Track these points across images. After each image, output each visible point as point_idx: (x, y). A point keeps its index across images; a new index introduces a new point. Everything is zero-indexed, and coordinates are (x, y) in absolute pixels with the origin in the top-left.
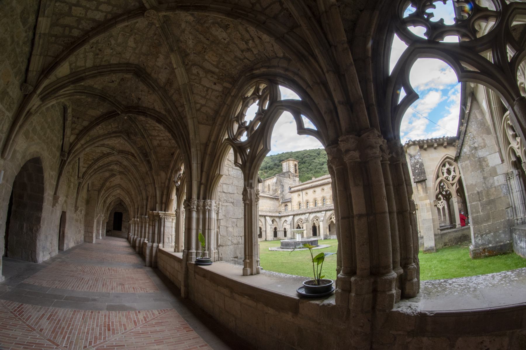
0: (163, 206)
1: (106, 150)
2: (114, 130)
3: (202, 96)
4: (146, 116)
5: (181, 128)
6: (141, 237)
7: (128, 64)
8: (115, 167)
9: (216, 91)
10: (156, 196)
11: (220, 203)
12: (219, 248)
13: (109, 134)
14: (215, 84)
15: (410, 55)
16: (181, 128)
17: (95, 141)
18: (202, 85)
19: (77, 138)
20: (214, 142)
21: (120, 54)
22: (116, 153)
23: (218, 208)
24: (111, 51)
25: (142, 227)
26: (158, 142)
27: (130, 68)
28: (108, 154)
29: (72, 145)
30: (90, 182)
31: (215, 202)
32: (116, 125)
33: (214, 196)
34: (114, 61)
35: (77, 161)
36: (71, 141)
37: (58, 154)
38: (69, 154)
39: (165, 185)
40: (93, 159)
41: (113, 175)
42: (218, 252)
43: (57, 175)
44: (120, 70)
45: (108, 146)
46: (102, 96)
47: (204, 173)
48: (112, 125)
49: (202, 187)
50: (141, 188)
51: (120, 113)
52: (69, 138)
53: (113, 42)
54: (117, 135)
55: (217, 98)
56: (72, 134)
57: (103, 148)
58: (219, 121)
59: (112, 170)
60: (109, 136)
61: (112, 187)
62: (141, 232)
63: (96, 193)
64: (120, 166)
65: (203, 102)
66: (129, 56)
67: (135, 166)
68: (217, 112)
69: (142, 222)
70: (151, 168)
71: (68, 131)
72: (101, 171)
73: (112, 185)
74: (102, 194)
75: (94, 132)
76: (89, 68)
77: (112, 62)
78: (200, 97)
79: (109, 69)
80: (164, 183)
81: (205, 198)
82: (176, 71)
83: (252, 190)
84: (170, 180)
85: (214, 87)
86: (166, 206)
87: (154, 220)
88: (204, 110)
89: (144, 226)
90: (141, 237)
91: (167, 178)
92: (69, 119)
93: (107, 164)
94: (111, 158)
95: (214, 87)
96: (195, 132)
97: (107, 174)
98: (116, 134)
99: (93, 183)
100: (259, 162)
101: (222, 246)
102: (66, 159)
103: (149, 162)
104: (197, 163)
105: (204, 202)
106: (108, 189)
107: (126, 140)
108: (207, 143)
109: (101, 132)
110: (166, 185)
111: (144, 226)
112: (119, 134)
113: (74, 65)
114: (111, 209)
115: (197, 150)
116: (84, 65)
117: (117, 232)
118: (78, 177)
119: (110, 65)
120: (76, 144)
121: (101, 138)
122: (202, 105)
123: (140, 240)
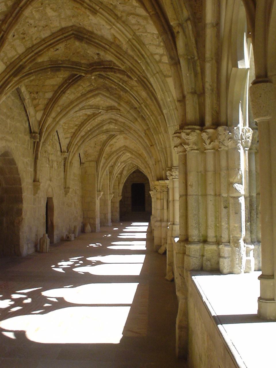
1: (89, 112)
2: (88, 89)
3: (156, 45)
7: (63, 30)
8: (112, 126)
13: (83, 95)
17: (67, 110)
18: (148, 33)
19: (44, 114)
21: (46, 26)
22: (103, 112)
24: (36, 29)
27: (67, 34)
28: (94, 115)
29: (41, 124)
30: (81, 152)
32: (88, 84)
34: (45, 34)
35: (56, 134)
36: (39, 118)
37: (27, 138)
38: (40, 133)
40: (76, 126)
41: (112, 137)
43: (33, 160)
44: (57, 41)
45: (91, 107)
46: (55, 67)
48: (83, 87)
51: (83, 74)
52: (35, 116)
53: (32, 21)
54: (94, 93)
56: (36, 111)
57: (84, 112)
59: (107, 131)
60: (85, 98)
61: (115, 151)
63: (93, 164)
64: (115, 123)
66: (57, 25)
71: (31, 111)
72: (90, 137)
73: (114, 149)
74: (101, 165)
75: (65, 99)
76: (22, 54)
77: (43, 37)
78: (154, 47)
79: (45, 45)
92: (27, 101)
93: (97, 125)
94: (99, 119)
97: (104, 137)
98: (93, 92)
99: (85, 153)
102: (38, 140)
106: (110, 155)
109: (72, 97)
112: (96, 92)
113: (6, 58)
114: (124, 180)
116: (16, 53)
118: (61, 152)
119: (44, 40)
120: (45, 121)
121: (75, 104)
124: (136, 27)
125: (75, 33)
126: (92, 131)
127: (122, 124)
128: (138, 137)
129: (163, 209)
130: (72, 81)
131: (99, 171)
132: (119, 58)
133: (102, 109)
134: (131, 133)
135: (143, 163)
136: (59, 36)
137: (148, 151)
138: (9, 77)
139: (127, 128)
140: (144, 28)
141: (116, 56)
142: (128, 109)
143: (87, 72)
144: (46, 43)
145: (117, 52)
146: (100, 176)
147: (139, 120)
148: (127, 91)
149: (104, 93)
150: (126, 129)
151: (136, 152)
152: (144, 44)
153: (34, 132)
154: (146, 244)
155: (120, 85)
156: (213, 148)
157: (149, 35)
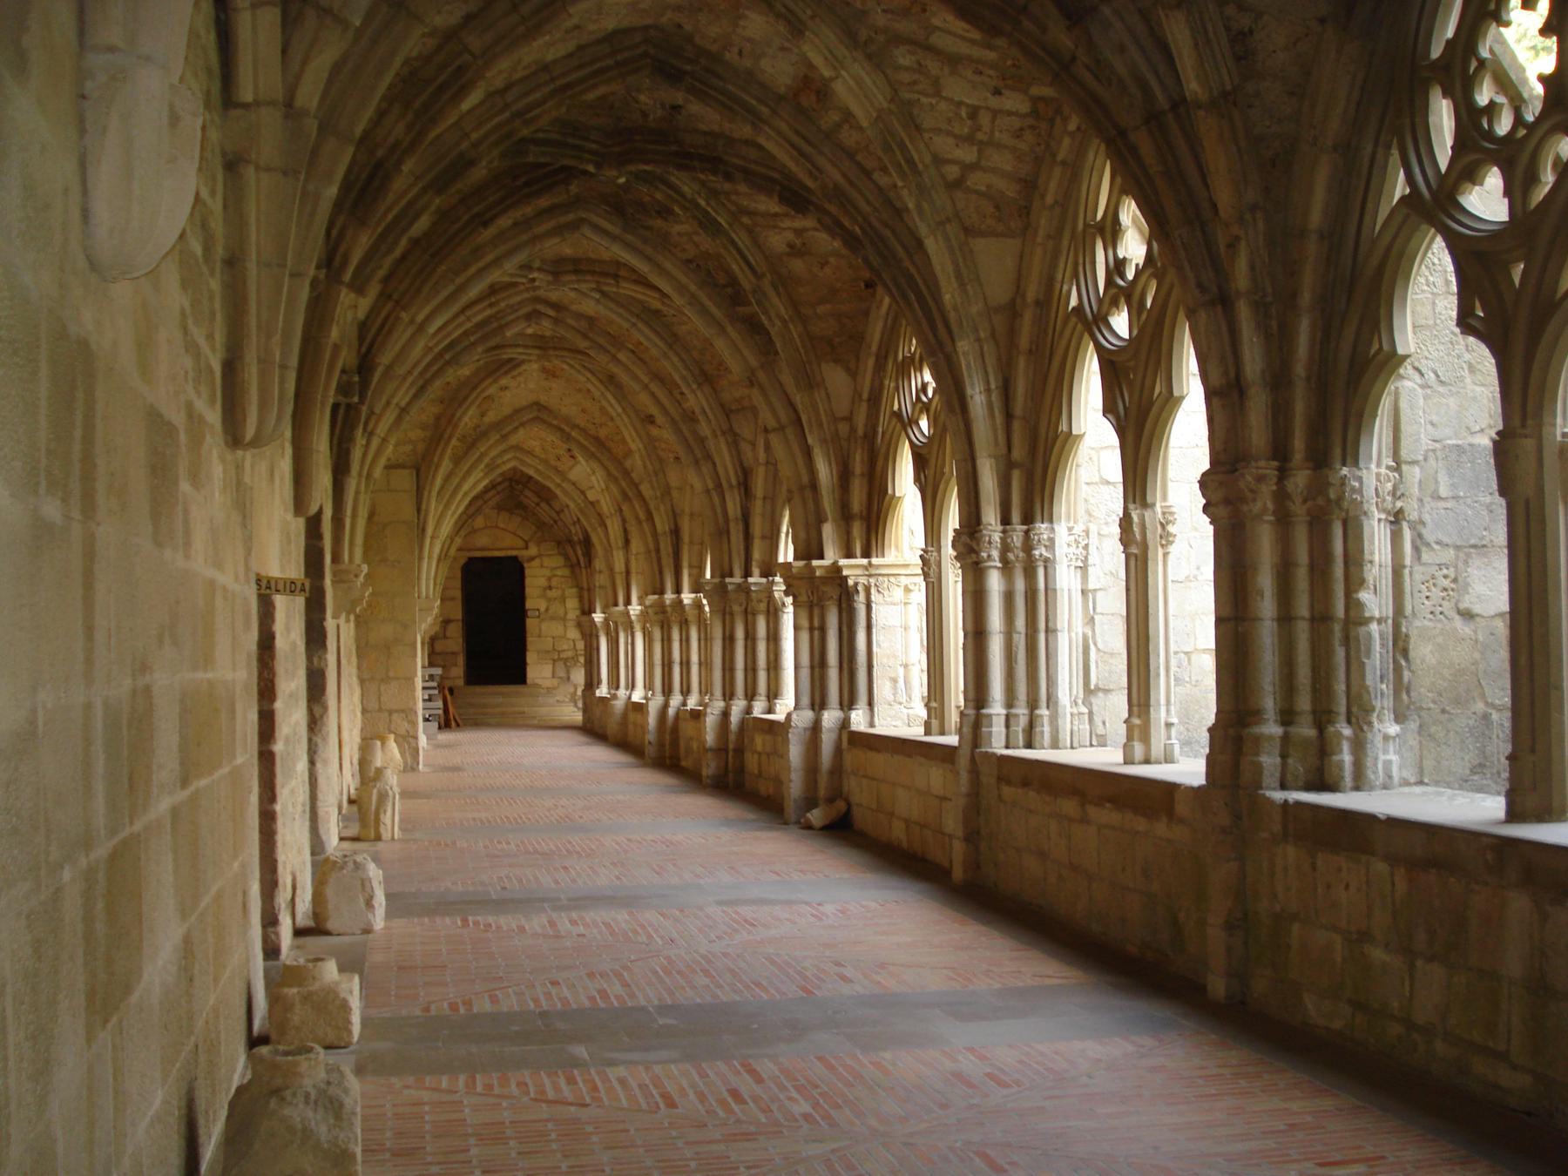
0: (857, 529)
4: (728, 177)
5: (901, 253)
6: (729, 695)
9: (1009, 113)
10: (814, 485)
11: (1093, 528)
12: (1093, 700)
14: (997, 92)
16: (901, 253)
17: (459, 280)
18: (946, 99)
19: (384, 296)
20: (1038, 303)
23: (1086, 547)
25: (729, 640)
26: (790, 236)
31: (1070, 529)
33: (1062, 507)
39: (853, 430)
42: (1091, 714)
47: (1017, 426)
49: (1016, 475)
50: (705, 429)
54: (563, 219)
55: (1018, 134)
58: (1044, 222)
61: (497, 425)
62: (728, 668)
64: (556, 321)
65: (967, 154)
67: (652, 317)
68: (1030, 186)
69: (725, 614)
70: (767, 349)
73: (491, 417)
78: (951, 141)
80: (849, 419)
81: (1028, 519)
82: (839, 87)
83: (1147, 514)
84: (875, 400)
86: (869, 525)
88: (977, 180)
89: (740, 634)
90: (729, 695)
91: (857, 394)
95: (994, 102)
96: (959, 276)
100: (1164, 414)
101: (1107, 691)
104: (988, 390)
105: (1027, 532)
110: (860, 432)
111: (740, 634)
112: (571, 217)
115: (978, 340)
117: (496, 696)
121: (490, 257)
122: (968, 168)
123: (726, 714)
124: (906, 77)
125: (652, 51)
126: (458, 349)
127: (583, 324)
128: (646, 380)
130: (527, 184)
131: (427, 511)
132: (802, 154)
133: (539, 269)
134: (618, 360)
135: (616, 480)
137: (687, 434)
139: (602, 341)
140: (936, 82)
141: (793, 146)
144: (553, 80)
145: (797, 133)
146: (429, 531)
147: (729, 329)
150: (601, 346)
151: (584, 431)
152: (918, 128)
155: (697, 205)
157: (943, 106)
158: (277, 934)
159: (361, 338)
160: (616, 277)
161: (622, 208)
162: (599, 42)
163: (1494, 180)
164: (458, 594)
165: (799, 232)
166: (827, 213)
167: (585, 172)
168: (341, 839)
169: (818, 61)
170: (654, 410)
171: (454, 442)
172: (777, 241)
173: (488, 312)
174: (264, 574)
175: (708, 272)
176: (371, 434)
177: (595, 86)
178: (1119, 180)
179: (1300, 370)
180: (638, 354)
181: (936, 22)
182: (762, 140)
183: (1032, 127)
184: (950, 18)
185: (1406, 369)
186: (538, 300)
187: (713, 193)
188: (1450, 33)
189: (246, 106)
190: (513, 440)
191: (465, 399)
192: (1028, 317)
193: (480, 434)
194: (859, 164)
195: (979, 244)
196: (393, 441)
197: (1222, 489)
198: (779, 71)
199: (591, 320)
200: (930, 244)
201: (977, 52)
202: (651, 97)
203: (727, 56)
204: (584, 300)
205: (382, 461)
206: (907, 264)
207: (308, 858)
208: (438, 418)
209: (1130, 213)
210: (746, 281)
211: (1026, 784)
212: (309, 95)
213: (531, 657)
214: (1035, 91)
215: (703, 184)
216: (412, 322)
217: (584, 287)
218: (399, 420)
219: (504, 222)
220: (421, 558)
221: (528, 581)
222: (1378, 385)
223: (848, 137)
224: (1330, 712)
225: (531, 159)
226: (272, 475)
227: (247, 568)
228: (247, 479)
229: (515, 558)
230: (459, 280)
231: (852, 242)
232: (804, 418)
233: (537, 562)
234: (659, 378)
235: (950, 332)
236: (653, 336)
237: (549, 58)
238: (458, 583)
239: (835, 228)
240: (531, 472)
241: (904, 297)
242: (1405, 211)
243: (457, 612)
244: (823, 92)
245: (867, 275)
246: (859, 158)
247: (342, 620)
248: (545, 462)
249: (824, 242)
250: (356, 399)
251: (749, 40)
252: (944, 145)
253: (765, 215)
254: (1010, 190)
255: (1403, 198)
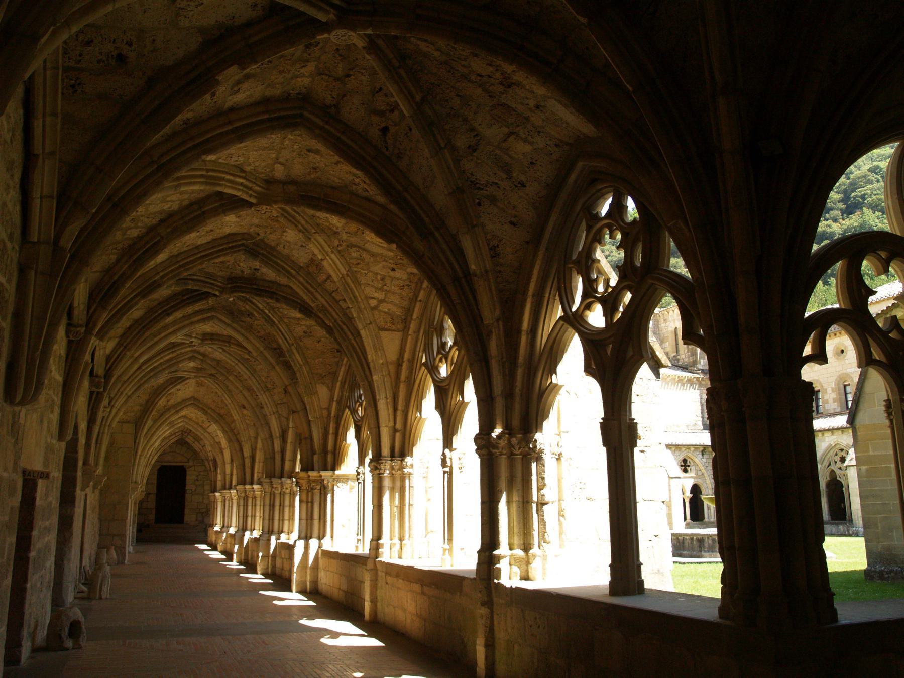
3: (376, 288)
4: (278, 300)
5: (351, 337)
14: (393, 270)
15: (449, 426)
16: (351, 337)
17: (156, 339)
19: (119, 344)
20: (409, 360)
47: (399, 413)
49: (398, 435)
54: (205, 316)
60: (187, 322)
61: (174, 406)
64: (202, 360)
65: (380, 296)
73: (172, 402)
78: (373, 290)
82: (325, 263)
85: (392, 273)
87: (310, 490)
91: (332, 399)
103: (287, 366)
107: (228, 325)
108: (398, 359)
111: (277, 503)
112: (209, 315)
120: (118, 359)
121: (170, 330)
122: (381, 301)
129: (312, 518)
136: (222, 245)
138: (136, 296)
142: (262, 349)
143: (223, 290)
145: (307, 282)
147: (277, 367)
148: (274, 322)
149: (223, 318)
153: (97, 376)
154: (823, 528)
155: (265, 313)
156: (521, 454)
158: (20, 652)
159: (107, 363)
160: (229, 342)
161: (233, 314)
162: (221, 238)
163: (598, 309)
164: (155, 482)
165: (309, 327)
166: (319, 317)
167: (215, 295)
168: (75, 598)
169: (316, 251)
170: (245, 403)
171: (153, 413)
172: (299, 330)
173: (171, 355)
174: (29, 468)
175: (268, 341)
176: (113, 407)
177: (219, 256)
178: (443, 310)
179: (517, 391)
180: (238, 377)
181: (368, 238)
182: (291, 285)
183: (409, 286)
184: (373, 235)
185: (562, 391)
186: (194, 351)
187: (272, 309)
188: (580, 249)
189: (34, 243)
190: (183, 413)
191: (160, 393)
192: (405, 365)
193: (167, 410)
194: (333, 298)
195: (384, 334)
196: (123, 410)
197: (483, 442)
198: (302, 257)
199: (219, 362)
200: (362, 332)
201: (385, 252)
202: (245, 265)
203: (279, 248)
204: (215, 352)
205: (117, 419)
206: (353, 341)
207: (48, 608)
208: (147, 401)
209: (449, 323)
210: (284, 346)
211: (397, 576)
212: (67, 242)
213: (187, 511)
214: (409, 270)
215: (268, 304)
216: (132, 356)
217: (215, 347)
218: (126, 402)
219: (178, 315)
220: (134, 465)
221: (188, 477)
222: (551, 397)
223: (329, 286)
224: (530, 544)
225: (190, 287)
226: (41, 421)
227: (15, 463)
228: (22, 421)
229: (183, 466)
230: (156, 339)
231: (330, 331)
232: (308, 408)
233: (192, 468)
234: (249, 389)
235: (370, 371)
236: (245, 370)
237: (199, 243)
238: (155, 477)
239: (323, 324)
240: (191, 428)
241: (352, 356)
242: (562, 323)
243: (154, 489)
244: (319, 266)
245: (337, 347)
246: (334, 295)
247: (89, 490)
248: (198, 424)
249: (320, 332)
250: (102, 390)
251: (288, 242)
252: (368, 291)
253: (294, 319)
254: (398, 312)
255: (561, 317)
